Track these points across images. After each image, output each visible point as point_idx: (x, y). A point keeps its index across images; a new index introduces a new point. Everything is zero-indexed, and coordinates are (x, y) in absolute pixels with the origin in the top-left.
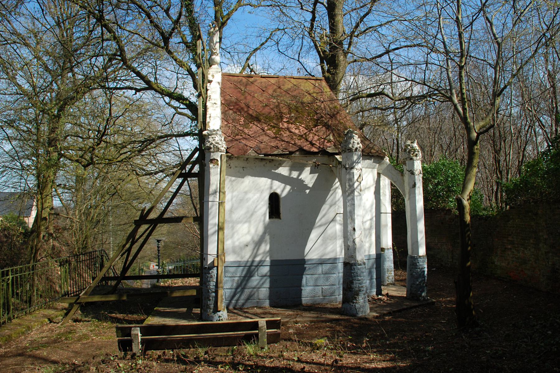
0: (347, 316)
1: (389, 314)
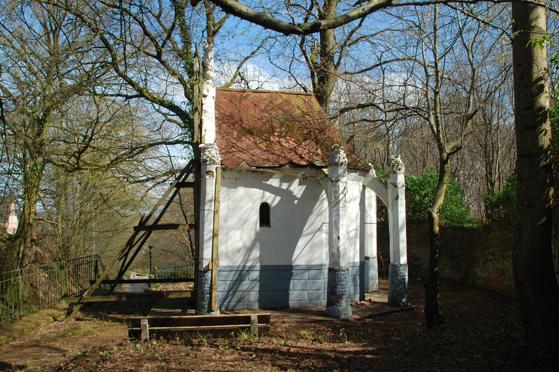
0: (331, 317)
1: (370, 317)
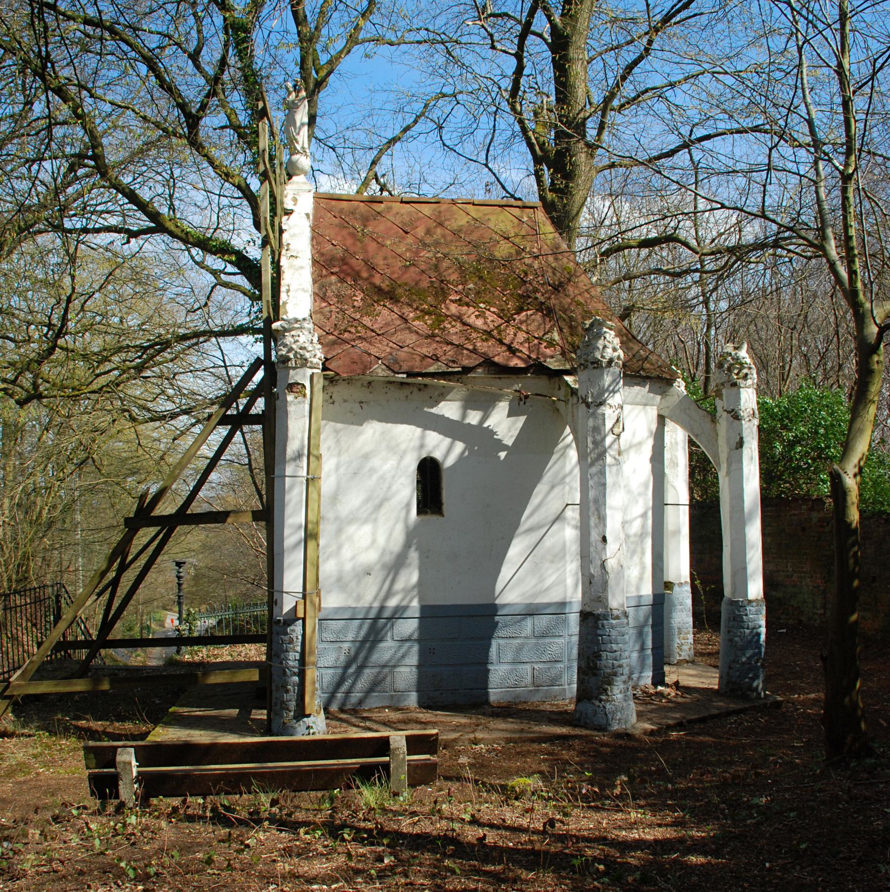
0: (587, 728)
1: (679, 726)
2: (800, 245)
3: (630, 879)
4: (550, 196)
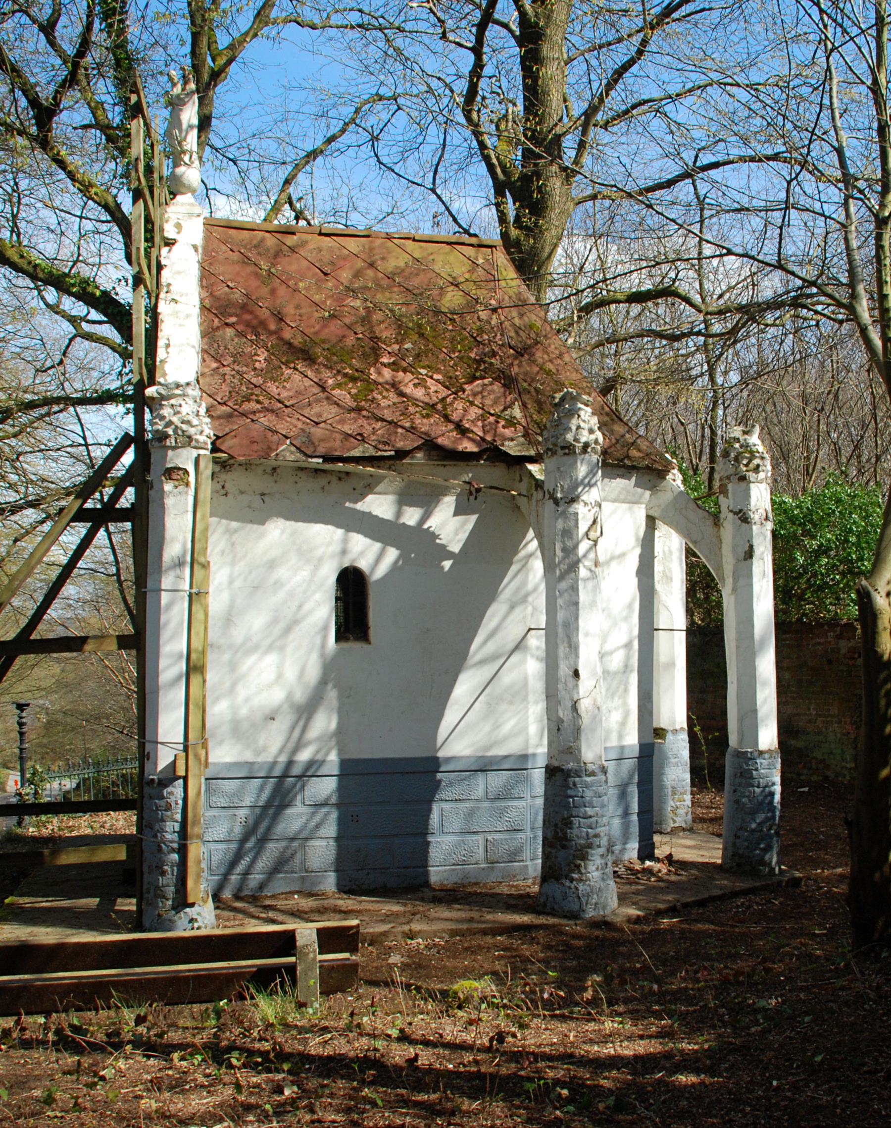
1: (672, 911)
2: (829, 305)
3: (601, 1106)
4: (514, 232)
